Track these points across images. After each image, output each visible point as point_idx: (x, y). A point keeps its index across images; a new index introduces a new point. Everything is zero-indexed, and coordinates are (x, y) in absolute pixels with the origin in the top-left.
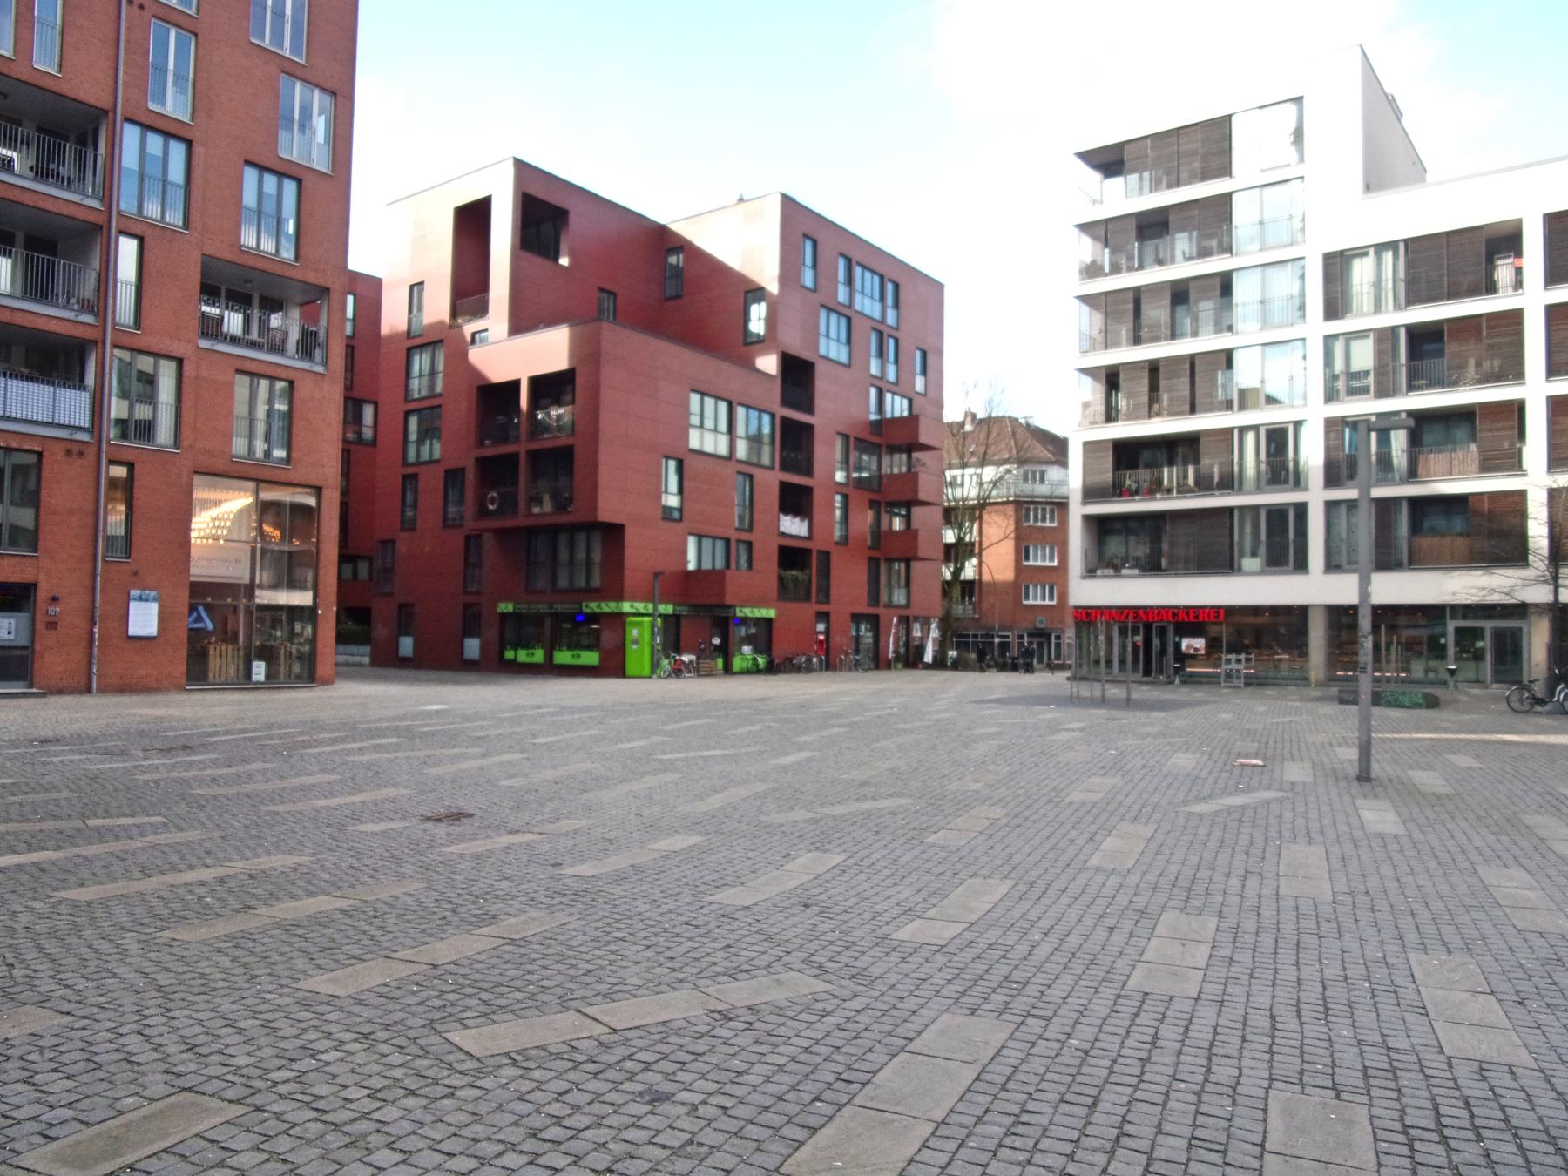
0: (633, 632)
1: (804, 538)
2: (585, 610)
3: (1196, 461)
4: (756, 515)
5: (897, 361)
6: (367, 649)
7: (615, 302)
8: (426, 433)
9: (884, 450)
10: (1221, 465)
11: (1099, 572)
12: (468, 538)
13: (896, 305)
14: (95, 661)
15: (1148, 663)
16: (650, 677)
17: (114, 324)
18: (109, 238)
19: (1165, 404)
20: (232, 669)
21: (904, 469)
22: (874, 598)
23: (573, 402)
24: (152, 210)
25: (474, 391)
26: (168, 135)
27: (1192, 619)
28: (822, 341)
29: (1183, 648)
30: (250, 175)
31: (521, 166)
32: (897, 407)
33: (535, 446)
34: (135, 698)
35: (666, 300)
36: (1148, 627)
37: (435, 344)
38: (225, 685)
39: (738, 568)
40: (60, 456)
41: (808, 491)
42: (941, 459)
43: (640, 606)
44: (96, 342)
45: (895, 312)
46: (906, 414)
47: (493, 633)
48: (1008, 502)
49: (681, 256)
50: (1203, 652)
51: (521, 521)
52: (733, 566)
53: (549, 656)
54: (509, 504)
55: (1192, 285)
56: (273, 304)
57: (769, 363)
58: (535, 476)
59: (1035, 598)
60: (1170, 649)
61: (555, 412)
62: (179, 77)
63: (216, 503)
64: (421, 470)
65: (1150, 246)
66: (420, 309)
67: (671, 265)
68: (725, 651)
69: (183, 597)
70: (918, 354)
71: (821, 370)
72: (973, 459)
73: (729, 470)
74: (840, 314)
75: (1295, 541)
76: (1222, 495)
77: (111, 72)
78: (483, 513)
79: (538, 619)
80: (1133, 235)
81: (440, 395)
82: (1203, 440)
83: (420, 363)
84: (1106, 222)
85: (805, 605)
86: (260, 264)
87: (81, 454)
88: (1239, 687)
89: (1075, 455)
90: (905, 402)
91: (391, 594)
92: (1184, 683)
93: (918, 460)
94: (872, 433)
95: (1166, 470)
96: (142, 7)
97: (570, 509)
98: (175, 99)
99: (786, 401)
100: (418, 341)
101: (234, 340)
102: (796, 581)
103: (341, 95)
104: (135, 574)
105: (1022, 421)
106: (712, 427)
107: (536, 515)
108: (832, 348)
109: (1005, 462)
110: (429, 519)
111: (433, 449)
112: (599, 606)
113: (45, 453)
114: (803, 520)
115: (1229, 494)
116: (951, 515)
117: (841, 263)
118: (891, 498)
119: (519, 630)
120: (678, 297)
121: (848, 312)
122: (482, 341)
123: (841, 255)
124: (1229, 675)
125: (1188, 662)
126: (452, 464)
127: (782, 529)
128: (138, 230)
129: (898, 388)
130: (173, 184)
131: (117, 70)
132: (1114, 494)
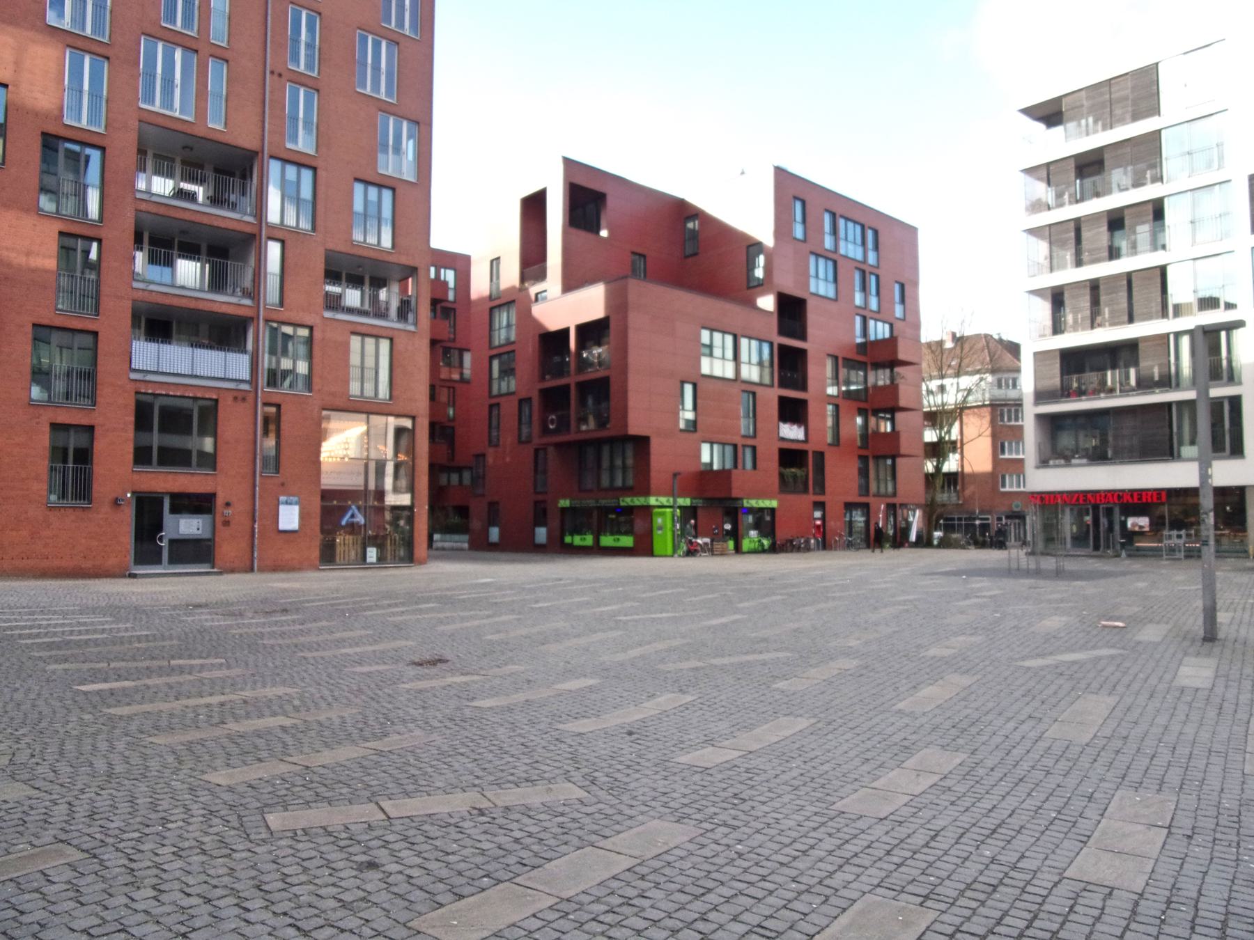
0: (658, 521)
1: (802, 441)
2: (622, 504)
3: (1136, 363)
4: (758, 425)
5: (878, 293)
6: (466, 537)
7: (645, 262)
8: (507, 372)
9: (869, 367)
10: (1160, 366)
11: (1051, 462)
12: (536, 451)
13: (876, 248)
14: (256, 549)
15: (1097, 538)
16: (672, 556)
17: (265, 305)
18: (260, 243)
19: (1107, 316)
20: (353, 553)
21: (888, 382)
22: (865, 490)
23: (608, 343)
24: (291, 221)
25: (537, 338)
26: (300, 165)
27: (1136, 501)
28: (812, 282)
29: (1129, 525)
30: (359, 188)
31: (568, 163)
32: (880, 331)
33: (582, 378)
34: (282, 575)
35: (687, 257)
36: (1096, 508)
37: (510, 303)
38: (347, 565)
39: (744, 468)
40: (230, 401)
41: (804, 403)
42: (920, 371)
43: (664, 500)
44: (252, 319)
45: (875, 253)
46: (887, 335)
47: (556, 523)
48: (984, 406)
49: (697, 222)
50: (1147, 529)
51: (572, 437)
52: (740, 466)
53: (597, 540)
54: (564, 424)
55: (1126, 212)
56: (379, 282)
57: (767, 302)
58: (582, 402)
59: (1011, 486)
60: (1117, 528)
61: (597, 351)
62: (307, 123)
63: (342, 430)
64: (502, 400)
65: (1088, 182)
66: (498, 278)
67: (690, 230)
68: (736, 535)
69: (316, 503)
70: (897, 287)
71: (811, 305)
72: (950, 372)
73: (735, 390)
74: (827, 258)
75: (1230, 431)
76: (1162, 392)
77: (260, 124)
78: (545, 431)
79: (587, 512)
80: (1073, 175)
81: (513, 343)
82: (1141, 346)
83: (503, 318)
84: (1048, 165)
85: (805, 496)
86: (365, 253)
87: (244, 399)
88: (1179, 559)
89: (1027, 363)
90: (887, 327)
91: (483, 495)
92: (1129, 556)
93: (898, 374)
94: (858, 353)
95: (1109, 373)
96: (280, 75)
97: (608, 426)
98: (304, 138)
99: (782, 331)
100: (500, 302)
101: (350, 311)
102: (795, 477)
103: (422, 124)
104: (283, 484)
105: (996, 337)
106: (721, 356)
107: (583, 432)
108: (820, 285)
109: (978, 372)
110: (508, 439)
111: (510, 385)
112: (632, 501)
113: (221, 401)
114: (800, 427)
115: (1167, 391)
116: (934, 418)
117: (827, 218)
118: (876, 406)
119: (576, 520)
120: (695, 254)
121: (834, 256)
122: (545, 298)
123: (827, 210)
124: (1172, 550)
125: (1136, 538)
126: (523, 395)
127: (782, 435)
128: (280, 235)
129: (879, 316)
130: (304, 200)
131: (263, 122)
132: (1062, 396)
